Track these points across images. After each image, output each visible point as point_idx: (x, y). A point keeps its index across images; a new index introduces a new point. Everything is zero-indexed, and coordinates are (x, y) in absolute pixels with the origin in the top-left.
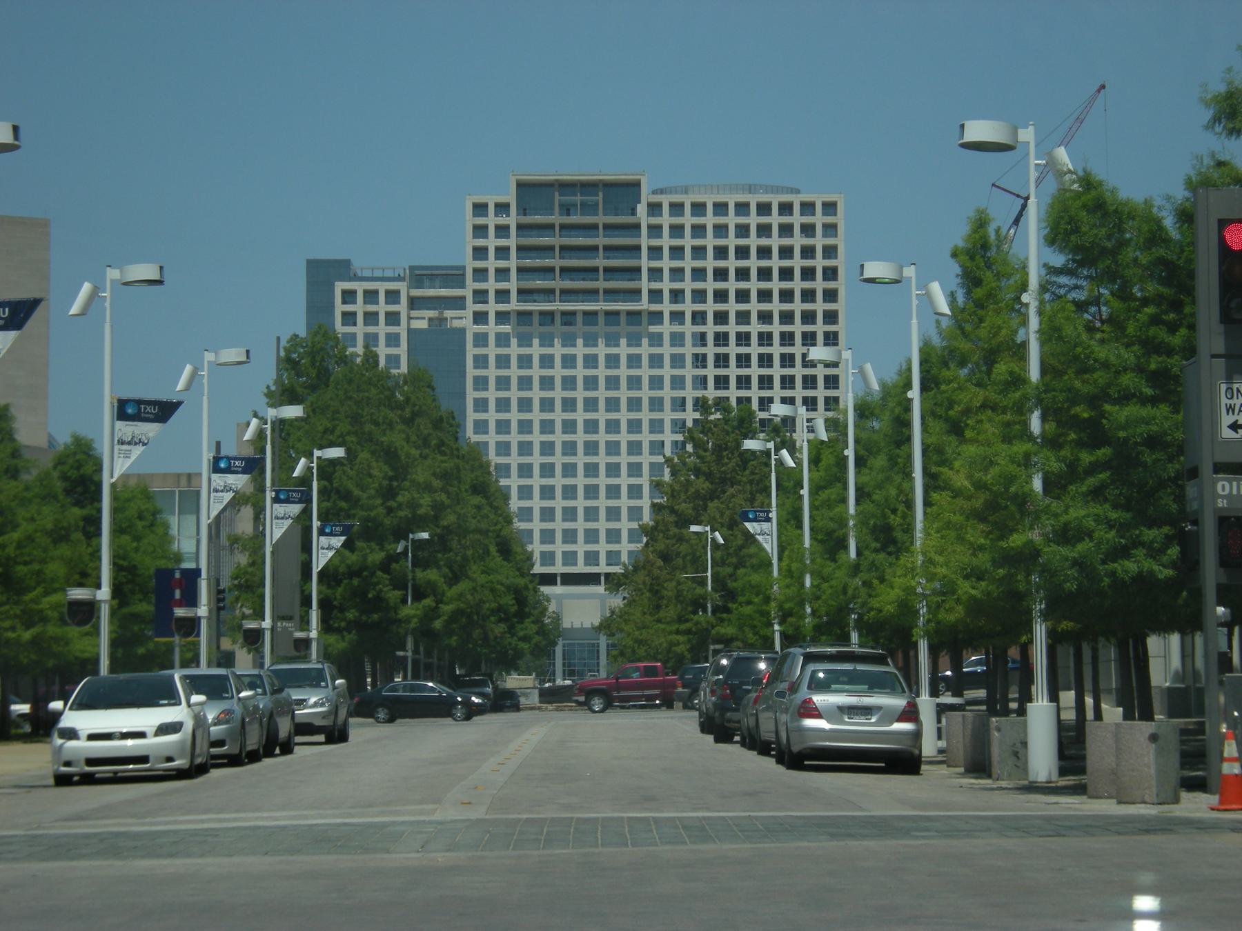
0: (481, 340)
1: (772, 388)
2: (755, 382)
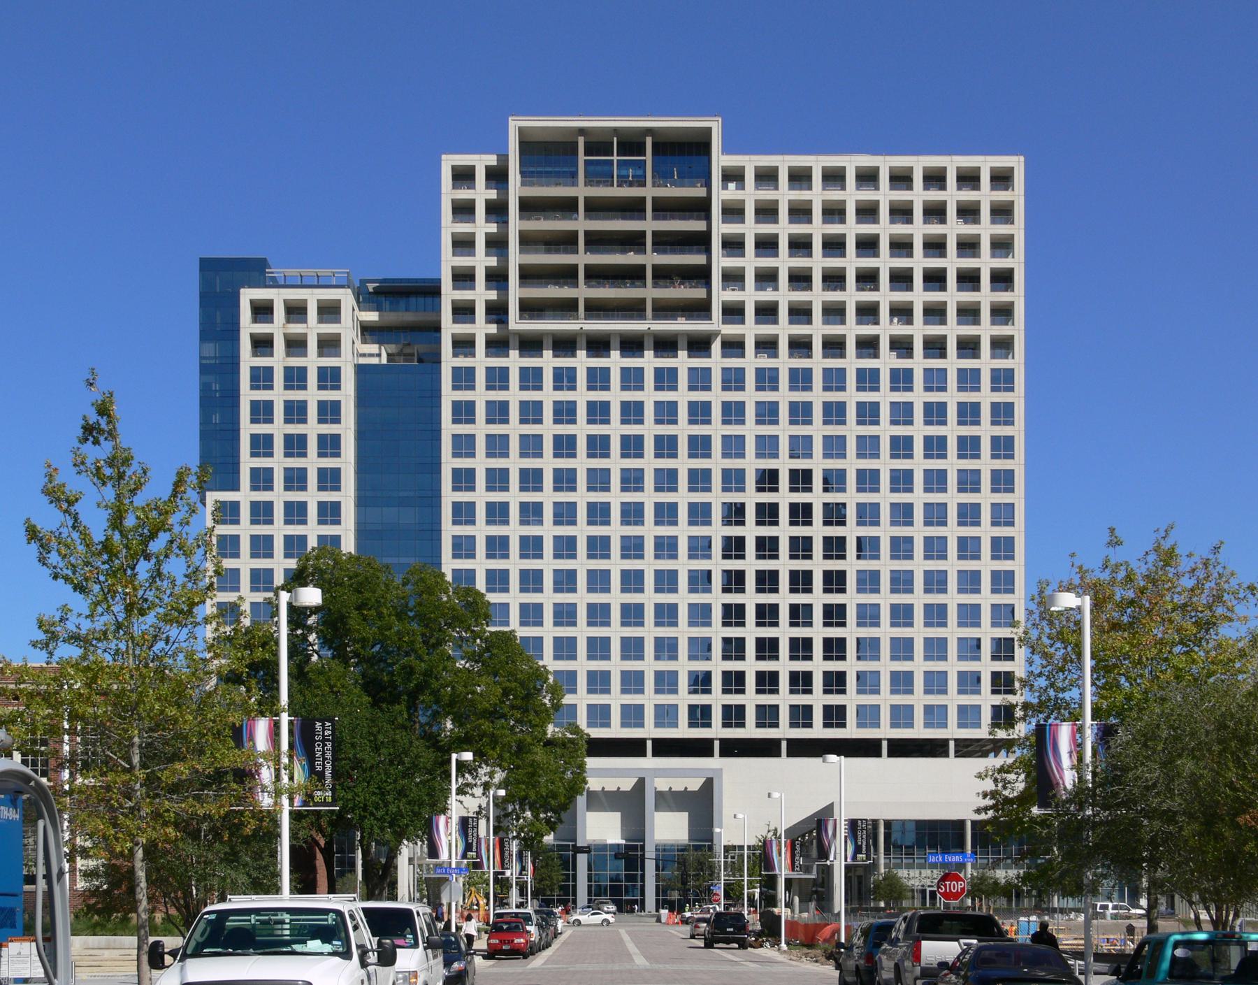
1: (911, 456)
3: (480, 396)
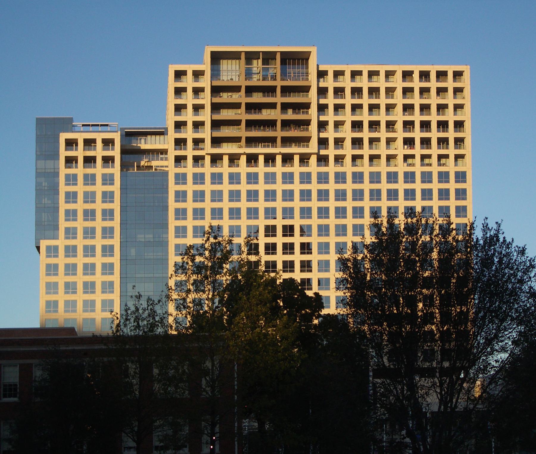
0: (181, 179)
2: (80, 269)
3: (190, 188)
